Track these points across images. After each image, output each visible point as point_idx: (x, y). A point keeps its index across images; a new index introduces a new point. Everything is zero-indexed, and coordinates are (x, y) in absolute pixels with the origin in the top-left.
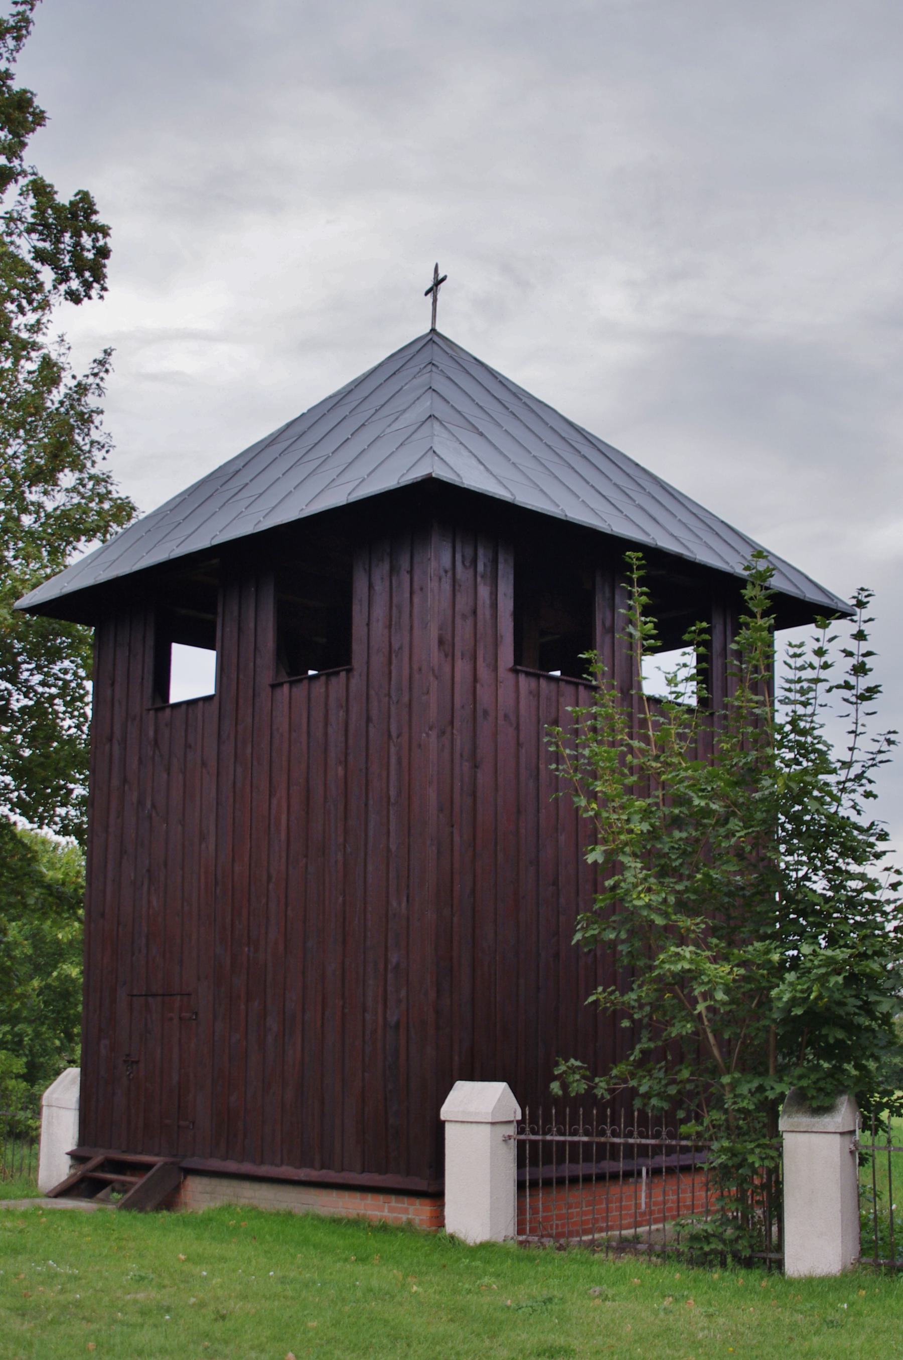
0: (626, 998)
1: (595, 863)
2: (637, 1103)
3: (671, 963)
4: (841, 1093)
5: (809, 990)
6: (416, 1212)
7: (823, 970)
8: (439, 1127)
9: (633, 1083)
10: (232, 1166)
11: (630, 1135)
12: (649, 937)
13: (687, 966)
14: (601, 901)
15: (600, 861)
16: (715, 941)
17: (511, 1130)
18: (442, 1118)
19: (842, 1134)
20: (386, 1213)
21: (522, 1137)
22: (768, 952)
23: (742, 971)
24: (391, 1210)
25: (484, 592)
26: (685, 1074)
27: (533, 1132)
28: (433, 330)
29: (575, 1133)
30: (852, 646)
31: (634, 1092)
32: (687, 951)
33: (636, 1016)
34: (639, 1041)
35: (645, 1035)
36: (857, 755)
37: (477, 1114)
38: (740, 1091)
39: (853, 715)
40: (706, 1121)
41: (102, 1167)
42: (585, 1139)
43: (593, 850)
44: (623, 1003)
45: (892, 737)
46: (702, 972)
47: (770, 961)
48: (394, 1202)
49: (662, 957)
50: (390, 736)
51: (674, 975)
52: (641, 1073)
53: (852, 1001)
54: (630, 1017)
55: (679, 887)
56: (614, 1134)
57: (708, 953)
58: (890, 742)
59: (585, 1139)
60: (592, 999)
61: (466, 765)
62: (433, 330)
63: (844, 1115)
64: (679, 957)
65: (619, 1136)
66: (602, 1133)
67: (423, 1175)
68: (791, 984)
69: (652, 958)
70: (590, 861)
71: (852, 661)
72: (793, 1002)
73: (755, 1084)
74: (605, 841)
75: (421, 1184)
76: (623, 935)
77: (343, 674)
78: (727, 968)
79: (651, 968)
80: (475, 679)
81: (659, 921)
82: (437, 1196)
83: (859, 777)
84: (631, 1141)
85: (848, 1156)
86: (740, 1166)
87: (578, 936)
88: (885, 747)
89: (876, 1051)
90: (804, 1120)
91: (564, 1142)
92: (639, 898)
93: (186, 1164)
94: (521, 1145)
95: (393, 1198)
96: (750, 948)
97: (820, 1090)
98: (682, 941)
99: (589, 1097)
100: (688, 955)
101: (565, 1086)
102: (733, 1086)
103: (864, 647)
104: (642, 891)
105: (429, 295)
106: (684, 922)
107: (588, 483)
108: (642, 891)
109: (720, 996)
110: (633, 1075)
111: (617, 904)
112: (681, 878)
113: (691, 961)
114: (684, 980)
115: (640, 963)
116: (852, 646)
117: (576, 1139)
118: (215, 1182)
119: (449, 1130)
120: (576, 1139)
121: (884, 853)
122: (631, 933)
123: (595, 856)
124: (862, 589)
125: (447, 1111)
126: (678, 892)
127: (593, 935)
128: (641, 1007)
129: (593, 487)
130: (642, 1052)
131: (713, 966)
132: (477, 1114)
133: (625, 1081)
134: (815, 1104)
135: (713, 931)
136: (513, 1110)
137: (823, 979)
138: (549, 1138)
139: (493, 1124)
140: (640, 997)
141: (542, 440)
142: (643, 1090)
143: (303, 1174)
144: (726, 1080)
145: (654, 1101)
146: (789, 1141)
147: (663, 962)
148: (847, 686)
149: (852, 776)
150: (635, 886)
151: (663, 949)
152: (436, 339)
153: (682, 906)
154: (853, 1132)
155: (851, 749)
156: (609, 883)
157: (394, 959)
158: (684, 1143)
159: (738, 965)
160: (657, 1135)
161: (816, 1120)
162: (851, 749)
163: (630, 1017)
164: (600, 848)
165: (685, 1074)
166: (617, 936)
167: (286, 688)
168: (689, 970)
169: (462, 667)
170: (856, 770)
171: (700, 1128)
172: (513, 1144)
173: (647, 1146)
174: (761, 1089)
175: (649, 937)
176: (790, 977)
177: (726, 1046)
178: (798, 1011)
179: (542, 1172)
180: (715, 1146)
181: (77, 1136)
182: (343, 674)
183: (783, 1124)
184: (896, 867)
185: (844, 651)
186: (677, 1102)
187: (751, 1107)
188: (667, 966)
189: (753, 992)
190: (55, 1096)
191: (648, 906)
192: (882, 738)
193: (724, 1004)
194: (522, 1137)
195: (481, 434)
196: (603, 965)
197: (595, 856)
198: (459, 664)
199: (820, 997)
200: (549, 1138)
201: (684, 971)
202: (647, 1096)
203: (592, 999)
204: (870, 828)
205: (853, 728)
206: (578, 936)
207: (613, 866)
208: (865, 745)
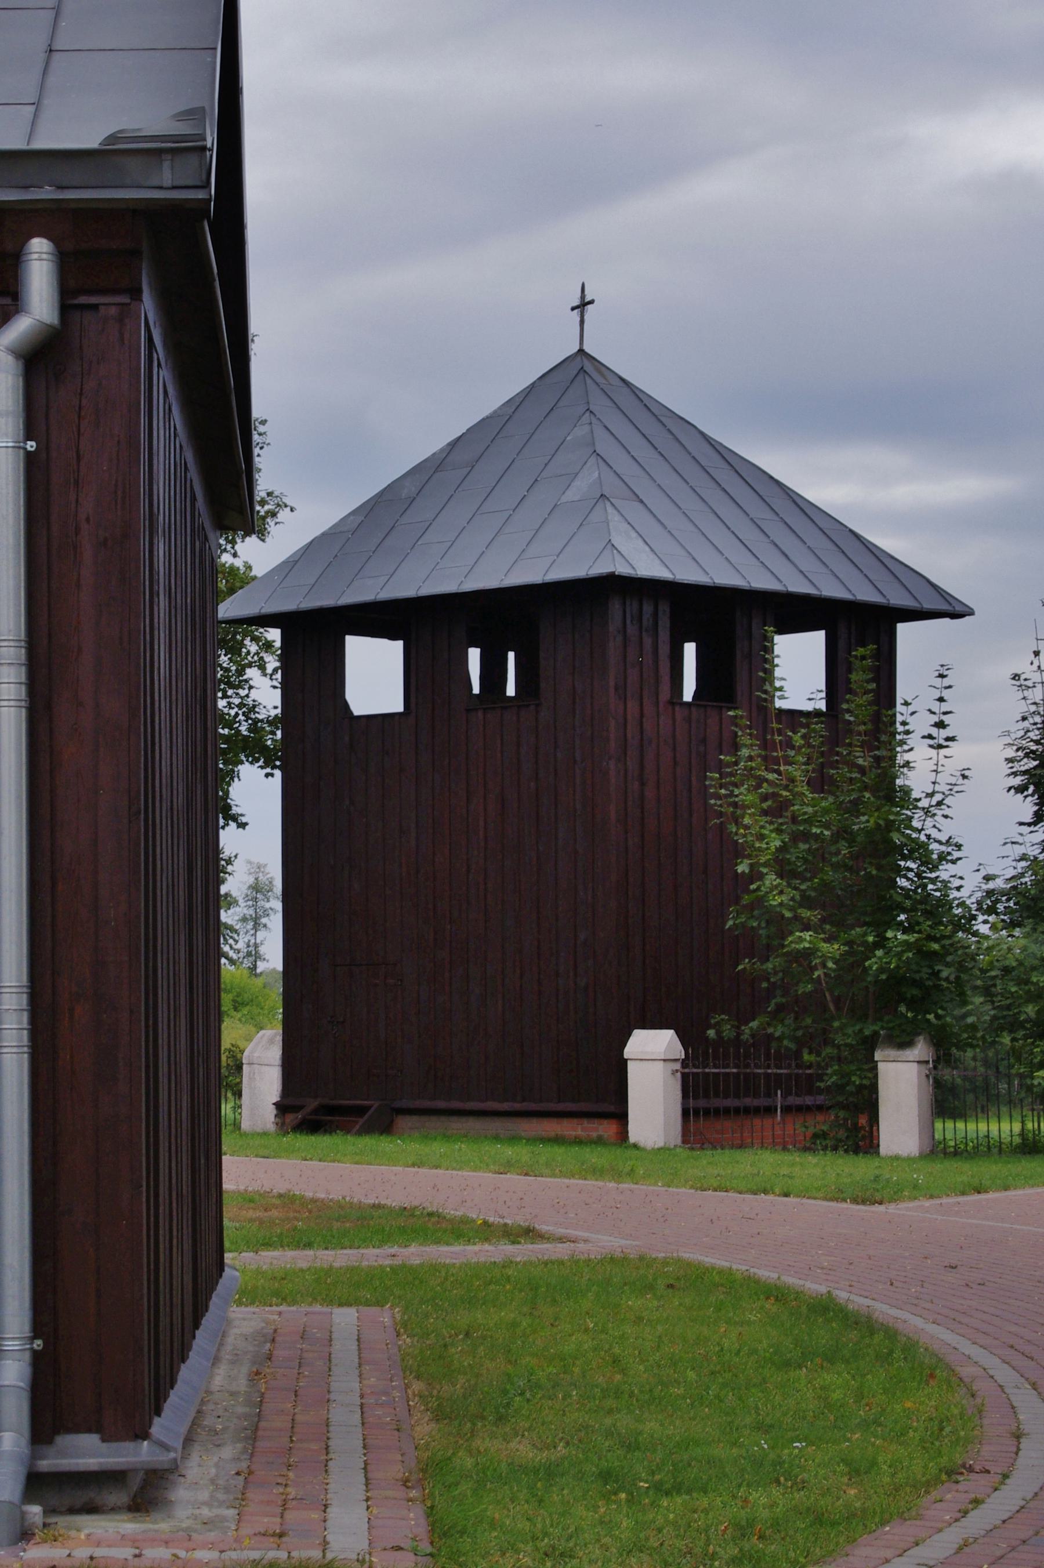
0: (764, 967)
1: (743, 872)
2: (774, 1044)
3: (797, 943)
4: (919, 1034)
5: (890, 963)
6: (607, 1129)
7: (899, 949)
8: (624, 1063)
9: (770, 1030)
10: (441, 1104)
11: (769, 1067)
12: (781, 926)
13: (807, 945)
14: (746, 899)
15: (747, 871)
16: (828, 927)
17: (678, 1066)
18: (625, 1057)
19: (918, 1062)
20: (579, 1132)
21: (686, 1070)
22: (865, 934)
23: (847, 948)
24: (583, 1129)
25: (648, 641)
26: (809, 1021)
27: (694, 1066)
28: (581, 351)
29: (727, 1066)
30: (936, 707)
31: (770, 1037)
32: (807, 935)
33: (772, 980)
34: (775, 997)
35: (778, 992)
36: (937, 788)
37: (652, 1055)
38: (846, 1032)
39: (935, 758)
40: (823, 1055)
41: (316, 1111)
42: (735, 1070)
43: (741, 862)
44: (764, 971)
45: (966, 773)
46: (818, 950)
47: (867, 941)
48: (586, 1123)
49: (790, 939)
50: (575, 762)
51: (798, 951)
52: (775, 1022)
53: (925, 970)
54: (768, 980)
55: (803, 887)
56: (757, 1066)
57: (822, 936)
58: (964, 777)
59: (735, 1070)
60: (740, 967)
61: (636, 785)
62: (581, 351)
63: (921, 1050)
64: (801, 940)
65: (760, 1068)
66: (747, 1066)
67: (610, 1102)
68: (880, 958)
69: (784, 938)
70: (739, 871)
71: (935, 719)
72: (881, 970)
73: (858, 1027)
74: (749, 857)
75: (612, 1109)
76: (763, 924)
77: (532, 707)
78: (836, 946)
79: (783, 946)
80: (642, 715)
81: (788, 914)
82: (621, 1117)
83: (940, 803)
84: (770, 1071)
85: (924, 1077)
86: (848, 1084)
87: (730, 923)
88: (960, 781)
89: (945, 1005)
90: (892, 1053)
91: (718, 1074)
92: (774, 899)
93: (398, 1104)
94: (685, 1077)
95: (585, 1121)
96: (853, 932)
97: (904, 1031)
98: (806, 928)
99: (737, 1041)
100: (808, 938)
101: (719, 1033)
102: (841, 1028)
103: (945, 707)
104: (775, 892)
105: (576, 311)
106: (805, 913)
107: (729, 529)
108: (775, 892)
109: (830, 964)
110: (769, 1024)
111: (759, 902)
112: (804, 880)
113: (810, 942)
114: (808, 954)
115: (775, 943)
116: (936, 707)
117: (727, 1070)
118: (424, 1118)
119: (630, 1065)
120: (727, 1070)
121: (960, 859)
122: (768, 922)
123: (742, 868)
124: (942, 666)
125: (628, 1051)
126: (802, 891)
127: (741, 923)
128: (776, 973)
129: (733, 533)
130: (776, 1004)
131: (825, 945)
132: (652, 1055)
133: (765, 1029)
134: (898, 1040)
135: (823, 920)
136: (678, 1051)
137: (899, 955)
138: (707, 1070)
139: (664, 1060)
140: (775, 966)
141: (688, 483)
142: (777, 1034)
143: (506, 1106)
144: (836, 1024)
145: (786, 1042)
146: (881, 1066)
147: (791, 942)
148: (930, 737)
149: (934, 803)
150: (772, 890)
151: (791, 933)
152: (588, 367)
153: (806, 901)
154: (927, 1062)
155: (934, 783)
156: (753, 887)
157: (582, 936)
158: (808, 1072)
159: (844, 945)
160: (789, 1067)
161: (900, 1052)
162: (934, 783)
163: (768, 980)
164: (747, 861)
165: (809, 1021)
166: (759, 924)
167: (480, 714)
168: (809, 948)
169: (632, 706)
170: (938, 797)
171: (818, 1059)
172: (679, 1075)
173: (781, 1074)
174: (861, 1031)
175: (781, 926)
176: (879, 953)
177: (837, 1001)
178: (884, 977)
179: (702, 1103)
180: (829, 1071)
181: (280, 1088)
182: (532, 707)
183: (878, 1055)
184: (959, 875)
185: (929, 710)
186: (801, 1043)
187: (854, 1043)
188: (793, 945)
189: (853, 962)
190: (256, 1055)
191: (781, 904)
192: (959, 774)
193: (834, 970)
194: (686, 1070)
195: (642, 502)
196: (746, 944)
197: (742, 868)
198: (630, 704)
199: (897, 967)
200: (707, 1070)
201: (804, 948)
202: (780, 1039)
203: (740, 967)
204: (948, 841)
205: (935, 768)
206: (730, 923)
207: (755, 875)
208: (944, 779)
